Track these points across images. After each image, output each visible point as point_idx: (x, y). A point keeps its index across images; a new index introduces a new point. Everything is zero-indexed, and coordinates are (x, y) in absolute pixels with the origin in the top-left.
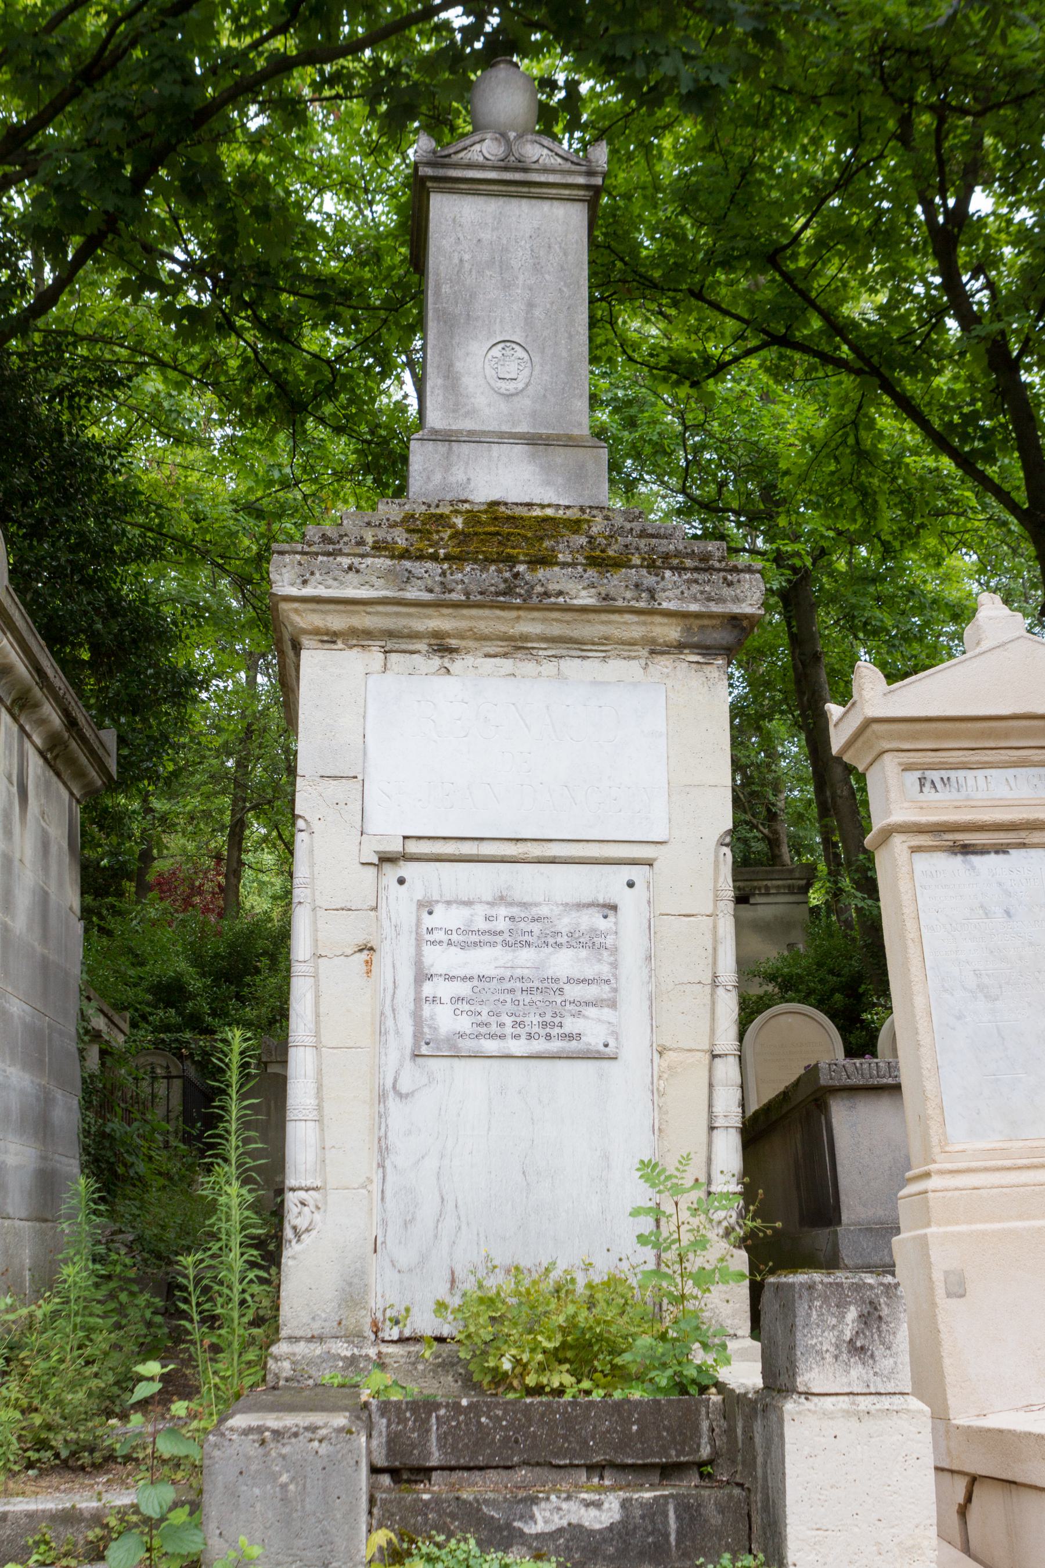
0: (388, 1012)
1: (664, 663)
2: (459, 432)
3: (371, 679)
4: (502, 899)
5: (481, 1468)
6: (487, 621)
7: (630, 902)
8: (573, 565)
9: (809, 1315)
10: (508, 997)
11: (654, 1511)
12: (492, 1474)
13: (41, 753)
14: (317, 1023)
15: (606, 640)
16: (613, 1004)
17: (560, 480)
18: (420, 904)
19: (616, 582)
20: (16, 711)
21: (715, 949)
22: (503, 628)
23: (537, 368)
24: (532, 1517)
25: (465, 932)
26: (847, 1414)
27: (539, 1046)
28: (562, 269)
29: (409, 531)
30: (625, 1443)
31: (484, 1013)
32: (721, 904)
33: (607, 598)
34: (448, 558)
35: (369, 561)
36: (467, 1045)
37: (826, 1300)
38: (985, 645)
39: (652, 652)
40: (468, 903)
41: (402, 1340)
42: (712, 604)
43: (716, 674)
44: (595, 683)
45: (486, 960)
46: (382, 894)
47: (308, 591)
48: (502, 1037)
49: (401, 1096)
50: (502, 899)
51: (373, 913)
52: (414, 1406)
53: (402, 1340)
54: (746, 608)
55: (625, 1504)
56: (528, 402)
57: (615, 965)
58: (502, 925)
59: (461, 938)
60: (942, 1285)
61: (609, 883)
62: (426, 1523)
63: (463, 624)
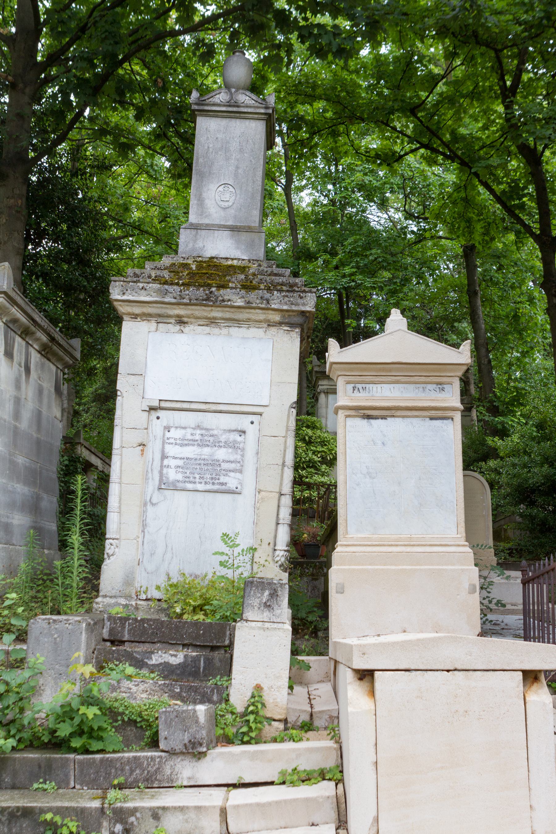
0: (150, 470)
1: (273, 330)
2: (202, 224)
3: (151, 334)
4: (198, 427)
5: (143, 642)
6: (199, 311)
7: (252, 431)
8: (235, 288)
9: (250, 592)
10: (198, 467)
11: (196, 660)
12: (147, 645)
13: (39, 352)
14: (121, 473)
15: (249, 320)
16: (241, 472)
17: (243, 247)
18: (165, 428)
19: (253, 296)
20: (24, 336)
21: (285, 451)
22: (206, 314)
23: (238, 196)
24: (151, 658)
25: (183, 440)
26: (260, 628)
27: (209, 487)
28: (252, 151)
29: (170, 272)
30: (198, 637)
31: (188, 473)
32: (289, 432)
33: (249, 302)
34: (183, 284)
35: (151, 285)
36: (180, 485)
37: (257, 587)
38: (386, 333)
39: (269, 325)
40: (185, 428)
41: (147, 600)
42: (293, 306)
43: (295, 335)
44: (243, 338)
45: (190, 452)
46: (150, 423)
47: (125, 297)
48: (195, 483)
49: (153, 505)
50: (198, 427)
51: (145, 431)
52: (121, 619)
53: (147, 600)
54: (308, 308)
55: (186, 656)
56: (233, 211)
57: (243, 456)
58: (197, 437)
59: (181, 442)
60: (335, 588)
61: (243, 422)
62: (113, 657)
63: (189, 312)
